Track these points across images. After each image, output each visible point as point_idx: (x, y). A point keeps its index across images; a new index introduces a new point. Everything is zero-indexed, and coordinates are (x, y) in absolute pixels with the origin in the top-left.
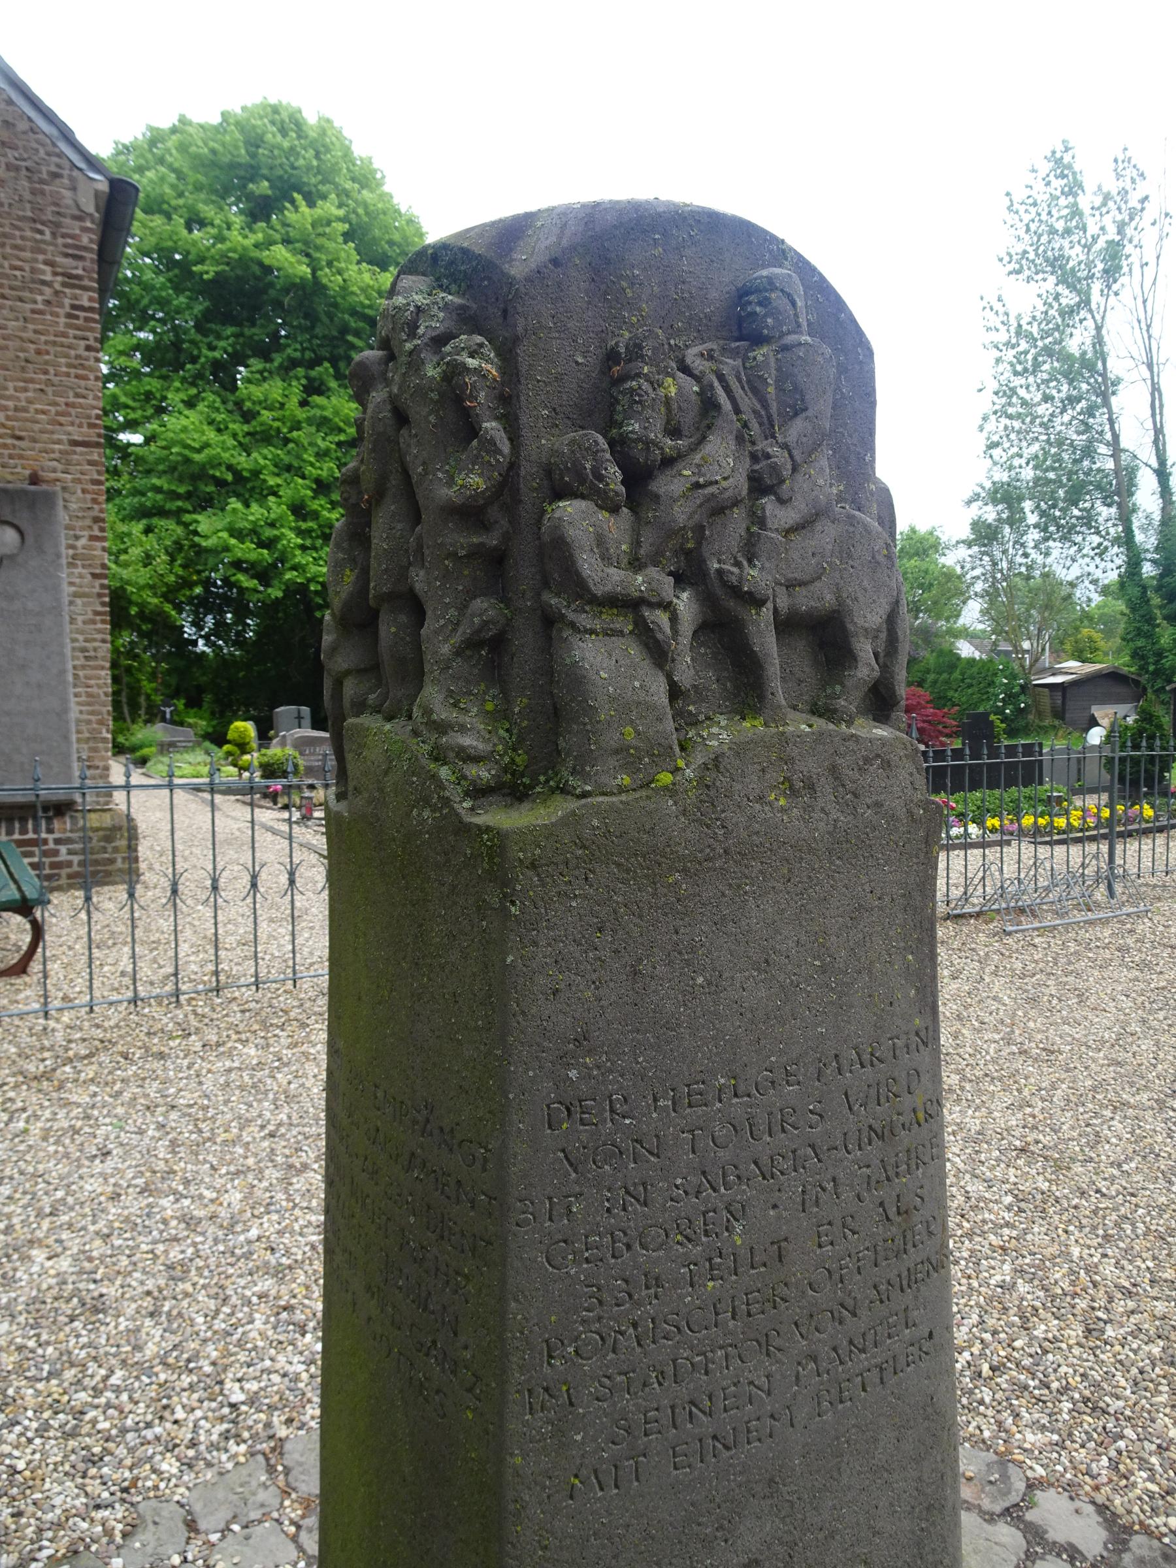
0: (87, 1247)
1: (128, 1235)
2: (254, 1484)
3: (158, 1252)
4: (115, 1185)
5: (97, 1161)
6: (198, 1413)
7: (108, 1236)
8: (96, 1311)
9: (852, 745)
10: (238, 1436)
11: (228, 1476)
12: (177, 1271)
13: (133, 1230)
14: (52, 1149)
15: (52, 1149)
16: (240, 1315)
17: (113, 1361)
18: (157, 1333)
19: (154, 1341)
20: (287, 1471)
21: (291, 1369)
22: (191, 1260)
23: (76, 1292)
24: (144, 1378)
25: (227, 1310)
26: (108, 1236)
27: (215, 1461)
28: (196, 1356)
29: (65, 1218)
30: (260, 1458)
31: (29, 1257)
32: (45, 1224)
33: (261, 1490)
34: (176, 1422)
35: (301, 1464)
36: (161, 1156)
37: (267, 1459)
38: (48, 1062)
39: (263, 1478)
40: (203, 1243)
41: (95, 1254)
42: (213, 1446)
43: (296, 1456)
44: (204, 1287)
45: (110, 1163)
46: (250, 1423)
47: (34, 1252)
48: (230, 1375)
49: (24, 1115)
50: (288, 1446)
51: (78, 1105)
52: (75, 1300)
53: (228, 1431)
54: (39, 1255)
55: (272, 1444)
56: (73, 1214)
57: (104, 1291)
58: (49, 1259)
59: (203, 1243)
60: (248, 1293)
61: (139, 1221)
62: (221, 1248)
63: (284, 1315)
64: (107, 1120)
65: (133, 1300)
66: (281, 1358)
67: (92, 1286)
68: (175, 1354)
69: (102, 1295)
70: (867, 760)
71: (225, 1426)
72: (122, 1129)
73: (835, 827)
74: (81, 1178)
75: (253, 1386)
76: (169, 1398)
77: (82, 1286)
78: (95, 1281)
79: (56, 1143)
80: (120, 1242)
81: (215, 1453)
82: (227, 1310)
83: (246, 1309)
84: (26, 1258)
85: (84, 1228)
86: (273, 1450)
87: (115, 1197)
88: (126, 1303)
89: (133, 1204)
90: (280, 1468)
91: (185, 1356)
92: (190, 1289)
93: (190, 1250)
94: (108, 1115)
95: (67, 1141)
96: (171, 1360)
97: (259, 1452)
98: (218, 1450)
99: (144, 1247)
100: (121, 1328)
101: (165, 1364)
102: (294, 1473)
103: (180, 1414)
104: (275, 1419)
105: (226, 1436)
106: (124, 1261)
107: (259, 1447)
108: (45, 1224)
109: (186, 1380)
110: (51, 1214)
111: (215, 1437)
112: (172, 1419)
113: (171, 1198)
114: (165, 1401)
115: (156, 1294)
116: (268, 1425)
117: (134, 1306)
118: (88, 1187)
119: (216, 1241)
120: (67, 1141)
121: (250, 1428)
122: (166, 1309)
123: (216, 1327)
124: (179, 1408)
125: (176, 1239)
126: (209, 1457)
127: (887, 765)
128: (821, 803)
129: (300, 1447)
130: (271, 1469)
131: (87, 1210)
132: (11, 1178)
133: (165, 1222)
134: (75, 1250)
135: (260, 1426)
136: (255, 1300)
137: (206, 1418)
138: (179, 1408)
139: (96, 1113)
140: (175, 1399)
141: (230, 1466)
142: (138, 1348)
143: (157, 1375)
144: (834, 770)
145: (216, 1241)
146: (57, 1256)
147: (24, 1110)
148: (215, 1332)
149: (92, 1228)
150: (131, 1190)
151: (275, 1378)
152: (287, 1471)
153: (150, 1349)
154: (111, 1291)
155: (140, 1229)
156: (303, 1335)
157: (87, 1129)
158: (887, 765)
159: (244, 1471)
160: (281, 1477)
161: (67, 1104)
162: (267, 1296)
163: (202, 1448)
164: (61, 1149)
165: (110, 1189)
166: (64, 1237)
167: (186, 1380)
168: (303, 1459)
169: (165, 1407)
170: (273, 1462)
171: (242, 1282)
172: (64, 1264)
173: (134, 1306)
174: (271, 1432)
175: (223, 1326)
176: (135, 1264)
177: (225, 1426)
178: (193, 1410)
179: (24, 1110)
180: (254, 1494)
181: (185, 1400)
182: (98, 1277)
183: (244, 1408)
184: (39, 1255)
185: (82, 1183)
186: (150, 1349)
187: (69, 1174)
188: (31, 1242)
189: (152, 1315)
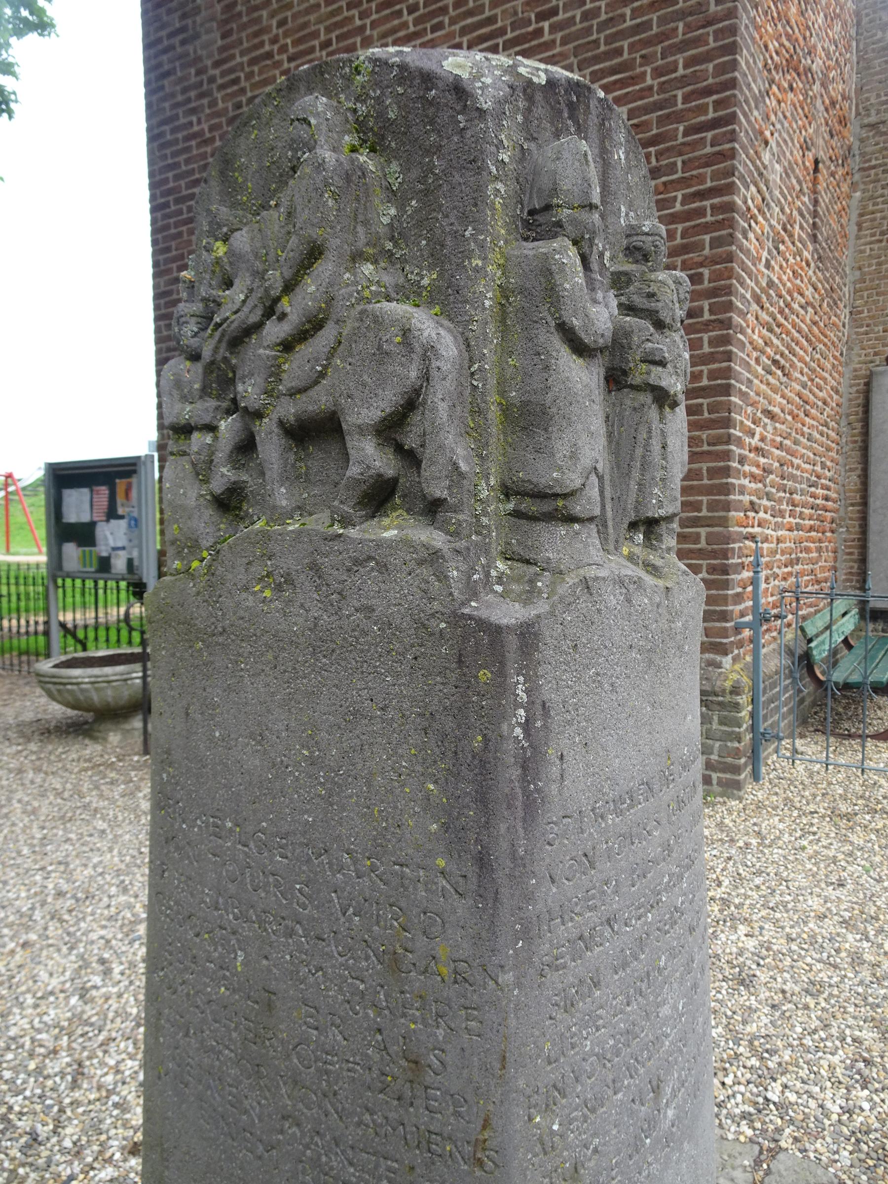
0: (774, 941)
1: (806, 946)
2: (738, 1162)
3: (814, 968)
4: (828, 909)
5: (832, 887)
6: (742, 1088)
7: (792, 940)
8: (742, 982)
9: (337, 546)
10: (752, 1121)
11: (725, 1142)
12: (814, 989)
13: (811, 944)
14: (809, 866)
15: (809, 866)
16: (829, 1044)
17: (724, 1021)
18: (765, 1020)
19: (760, 1024)
20: (768, 1172)
21: (829, 1104)
22: (830, 986)
23: (742, 966)
24: (730, 1042)
25: (823, 1034)
26: (792, 940)
27: (726, 1127)
28: (772, 1052)
29: (778, 915)
30: (757, 1148)
31: (736, 928)
32: (763, 913)
33: (740, 1170)
34: (723, 1084)
35: (781, 1176)
36: (878, 903)
37: (761, 1153)
38: (857, 808)
39: (746, 1163)
40: (850, 979)
41: (775, 948)
42: (729, 1116)
43: (782, 1167)
44: (823, 1009)
45: (840, 893)
46: (767, 1120)
47: (741, 927)
48: (784, 1079)
49: (812, 837)
50: (781, 1156)
51: (852, 843)
52: (737, 969)
53: (750, 1114)
54: (743, 929)
55: (772, 1146)
56: (785, 915)
57: (758, 973)
58: (746, 935)
59: (850, 979)
60: (848, 1032)
61: (820, 940)
62: (860, 990)
63: (861, 1065)
64: (863, 863)
65: (770, 989)
66: (829, 1094)
67: (754, 966)
68: (762, 1040)
69: (754, 976)
70: (357, 562)
71: (752, 1110)
72: (867, 871)
73: (316, 625)
74: (811, 894)
75: (793, 1097)
76: (731, 1065)
77: (748, 962)
78: (758, 965)
79: (815, 864)
80: (796, 948)
81: (729, 1121)
82: (823, 1034)
83: (838, 1043)
84: (734, 928)
85: (783, 928)
86: (770, 1150)
87: (822, 917)
88: (764, 989)
89: (830, 926)
90: (765, 1166)
91: (768, 1046)
92: (812, 1006)
93: (836, 979)
94: (866, 860)
95: (822, 865)
96: (756, 1043)
97: (759, 1143)
98: (733, 1121)
99: (809, 960)
100: (747, 1003)
101: (751, 1043)
102: (771, 1177)
103: (729, 1081)
104: (787, 1131)
105: (745, 1116)
106: (788, 961)
107: (760, 1140)
108: (763, 913)
109: (754, 1062)
110: (772, 909)
111: (737, 1111)
112: (722, 1079)
113: (858, 937)
114: (727, 1065)
115: (788, 995)
116: (779, 1130)
117: (767, 994)
118: (810, 903)
119: (861, 983)
120: (822, 865)
121: (764, 1123)
122: (784, 1008)
123: (805, 1041)
124: (731, 1076)
125: (836, 967)
126: (723, 1120)
127: (383, 567)
128: (300, 598)
129: (789, 1163)
130: (758, 1163)
131: (796, 917)
132: (768, 874)
133: (838, 951)
134: (765, 939)
135: (772, 1127)
136: (849, 1040)
137: (743, 1095)
138: (731, 1076)
139: (859, 854)
140: (734, 1068)
141: (731, 1136)
142: (745, 1022)
143: (739, 1045)
144: (314, 567)
145: (861, 983)
146: (752, 936)
147: (814, 834)
148: (802, 1044)
149: (788, 930)
150: (836, 918)
151: (812, 1104)
152: (768, 1172)
153: (752, 1028)
154: (763, 976)
155: (816, 946)
156: (862, 1089)
157: (843, 863)
158: (383, 567)
159: (739, 1148)
160: (761, 1173)
161: (846, 840)
162: (861, 1043)
163: (724, 1111)
164: (815, 869)
165: (823, 910)
166: (766, 926)
167: (754, 1062)
168: (784, 1173)
169: (725, 1069)
170: (763, 1157)
171: (851, 1021)
172: (751, 944)
173: (767, 994)
174: (777, 1137)
175: (810, 1043)
176: (792, 967)
177: (752, 1110)
178: (739, 1083)
179: (814, 834)
180: (733, 1168)
181: (739, 1074)
182: (762, 962)
183: (772, 1106)
184: (743, 929)
185: (809, 897)
186: (752, 1028)
187: (805, 888)
188: (746, 920)
189: (773, 1006)
